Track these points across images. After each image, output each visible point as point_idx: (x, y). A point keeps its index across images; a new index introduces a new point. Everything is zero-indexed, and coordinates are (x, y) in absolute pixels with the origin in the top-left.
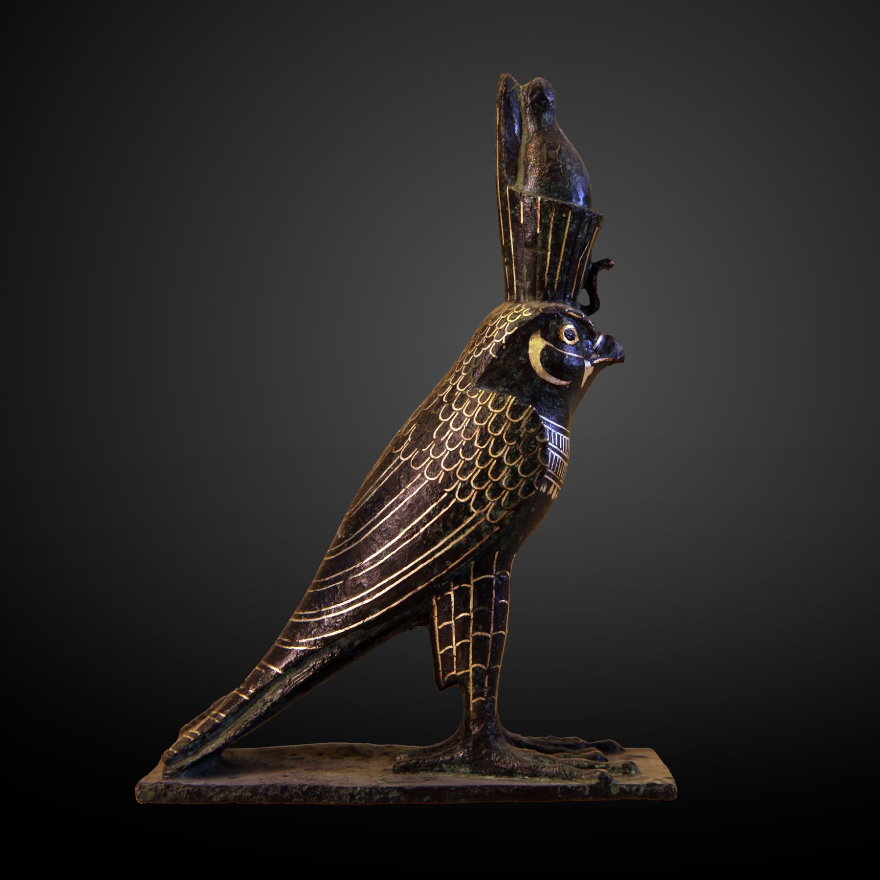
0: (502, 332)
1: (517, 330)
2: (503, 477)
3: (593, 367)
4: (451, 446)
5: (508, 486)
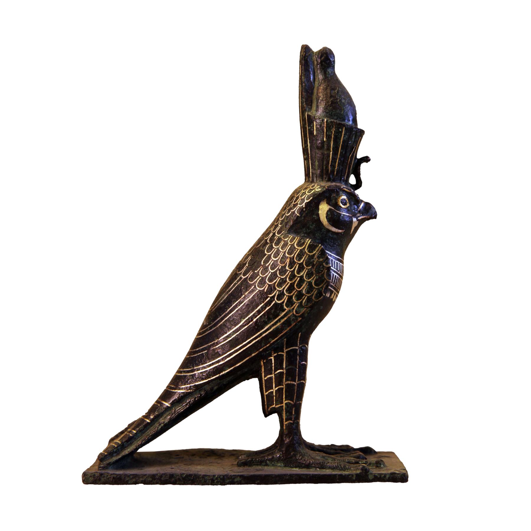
0: (303, 200)
1: (312, 199)
2: (303, 288)
3: (358, 222)
4: (272, 269)
5: (306, 293)
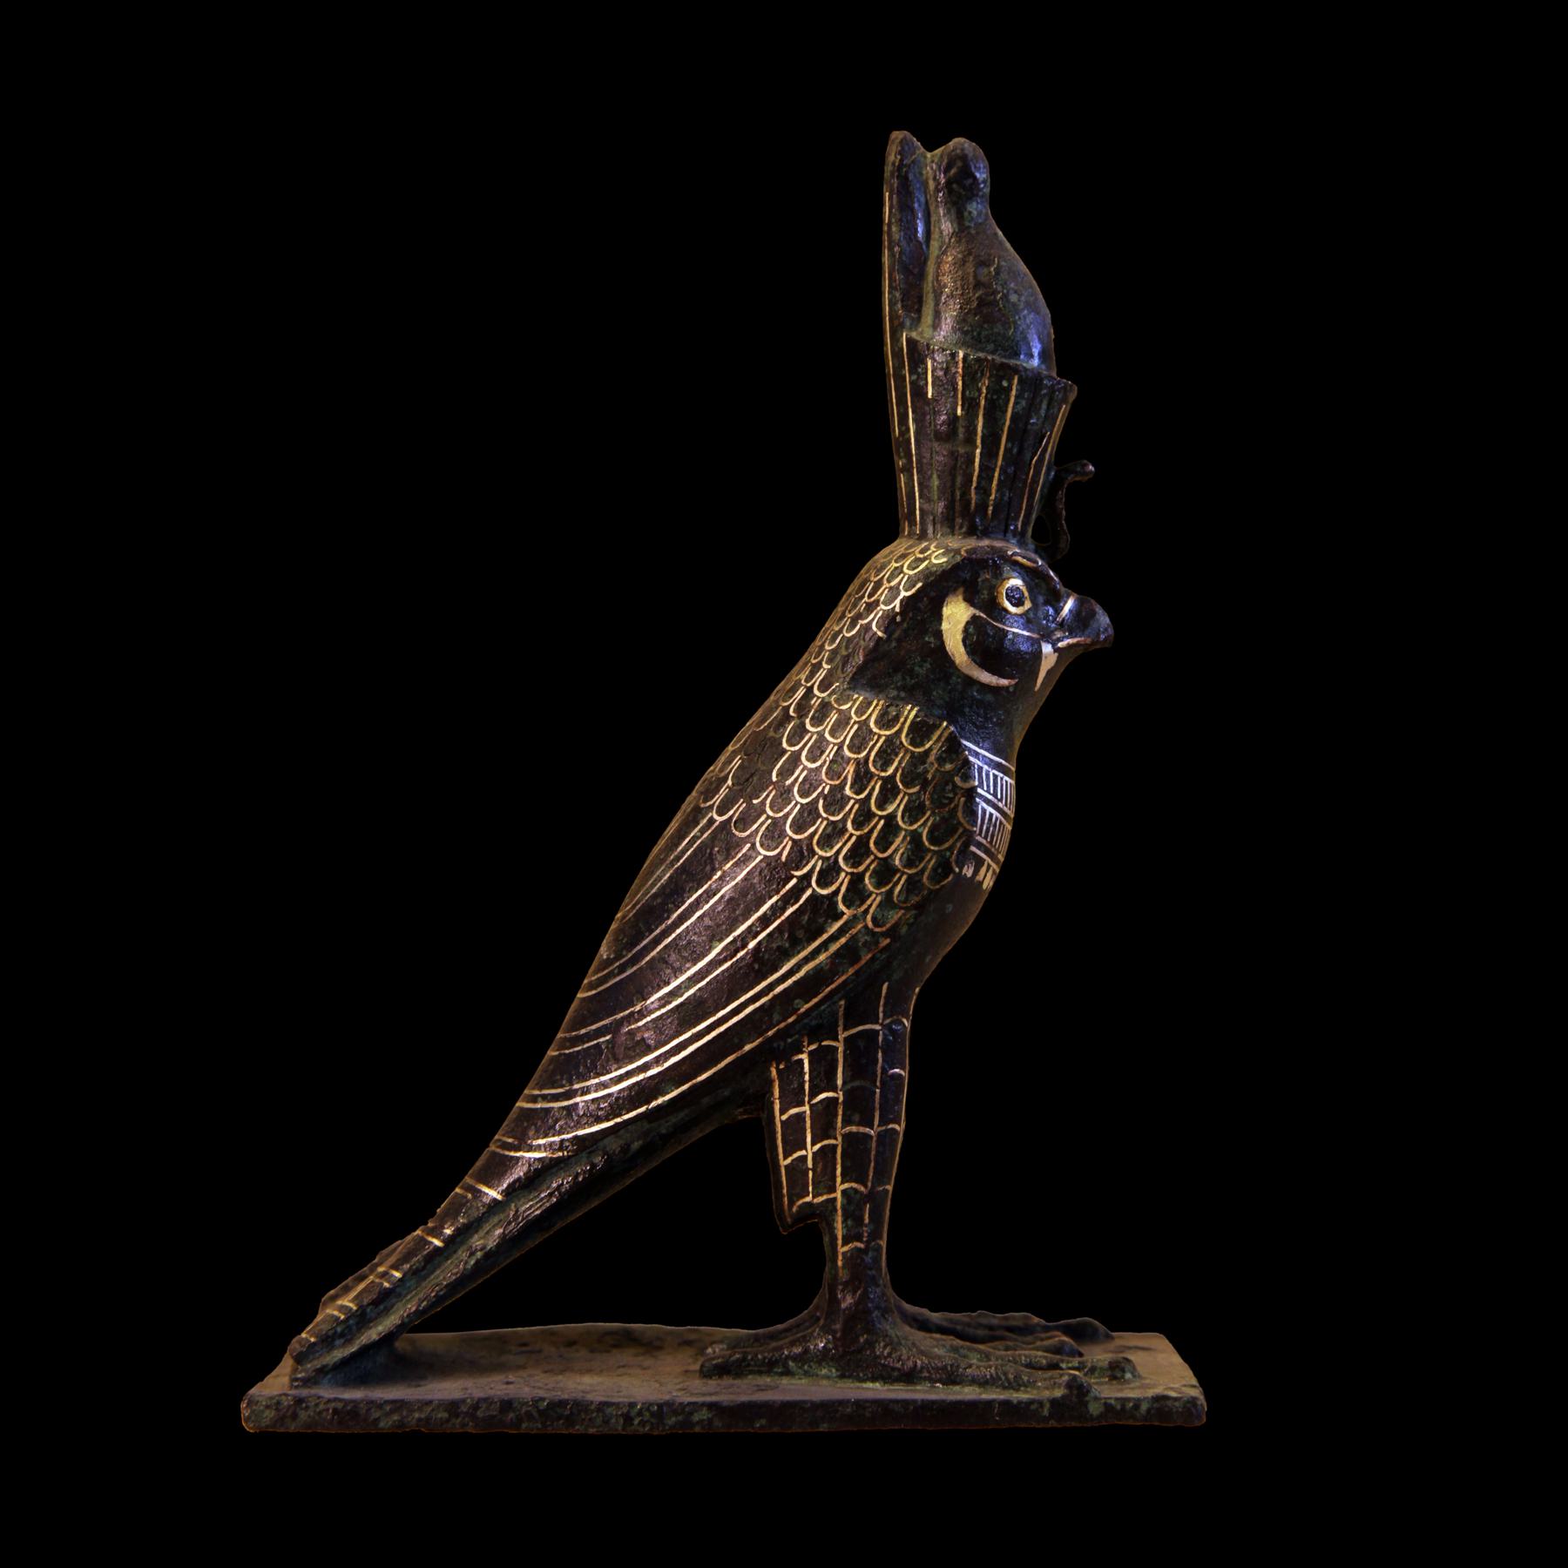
0: (894, 591)
1: (921, 587)
2: (896, 851)
3: (1056, 654)
4: (803, 794)
5: (905, 867)
